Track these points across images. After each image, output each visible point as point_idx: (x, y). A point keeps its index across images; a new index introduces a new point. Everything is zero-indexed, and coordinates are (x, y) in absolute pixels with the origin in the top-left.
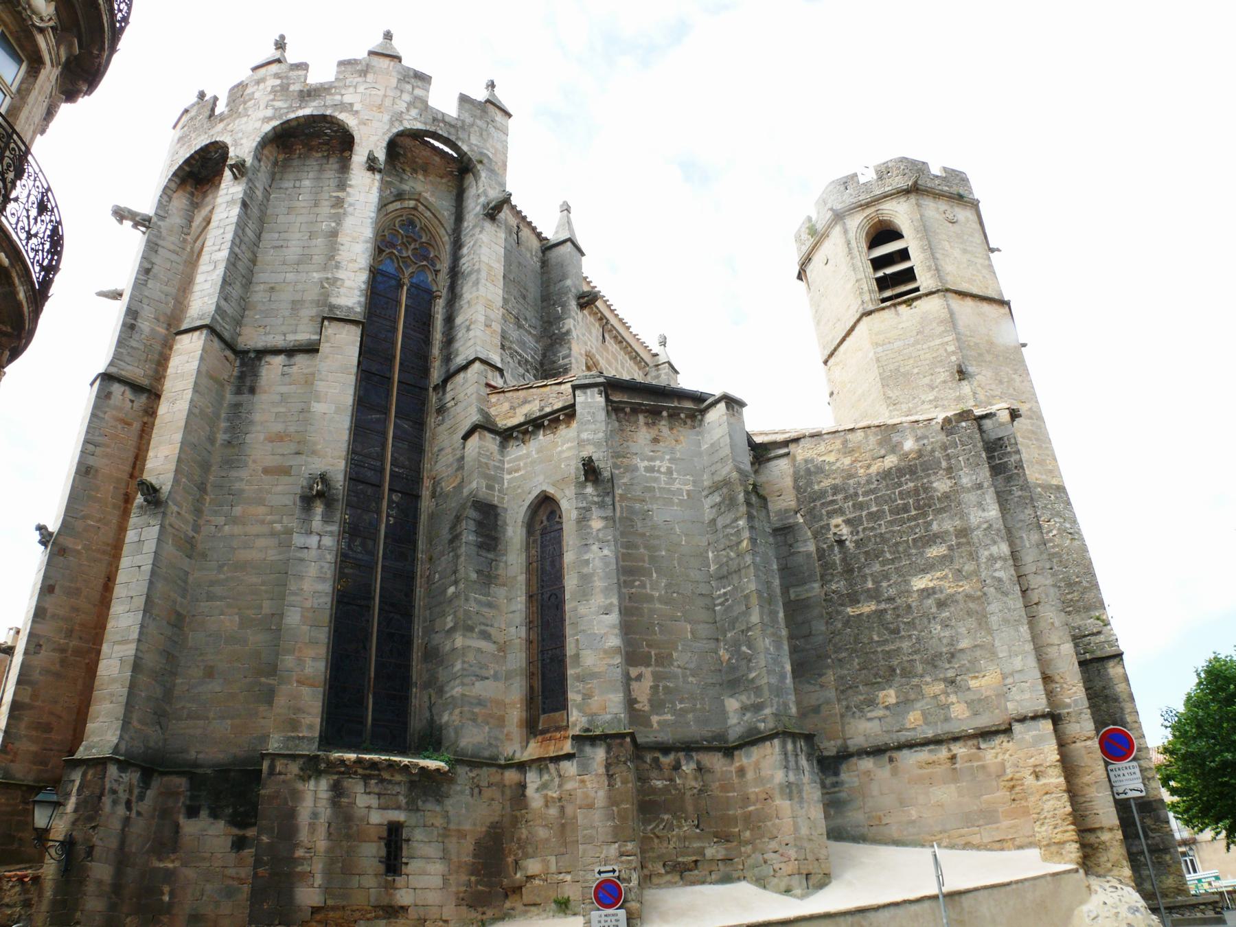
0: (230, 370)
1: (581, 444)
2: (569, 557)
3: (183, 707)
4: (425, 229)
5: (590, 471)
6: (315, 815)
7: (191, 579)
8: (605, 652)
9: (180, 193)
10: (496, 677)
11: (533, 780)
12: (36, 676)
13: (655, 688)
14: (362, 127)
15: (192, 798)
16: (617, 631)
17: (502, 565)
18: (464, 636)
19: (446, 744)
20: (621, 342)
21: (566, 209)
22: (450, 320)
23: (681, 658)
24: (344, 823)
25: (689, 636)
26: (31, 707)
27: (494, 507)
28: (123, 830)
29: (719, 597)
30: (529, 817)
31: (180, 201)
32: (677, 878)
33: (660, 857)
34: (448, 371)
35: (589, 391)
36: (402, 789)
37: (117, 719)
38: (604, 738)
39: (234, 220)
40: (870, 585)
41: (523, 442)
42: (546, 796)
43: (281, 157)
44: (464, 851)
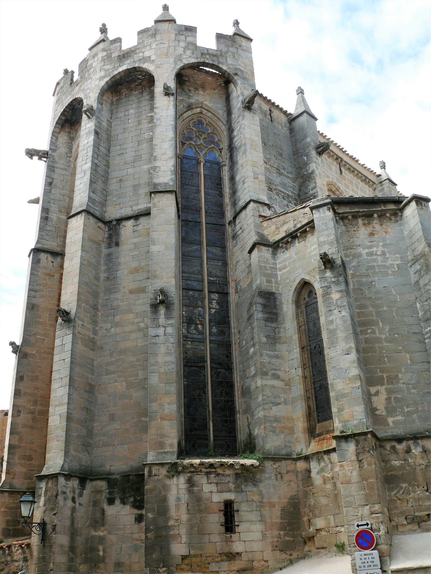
0: (102, 233)
1: (320, 245)
2: (322, 320)
3: (100, 440)
4: (209, 124)
5: (327, 262)
6: (178, 499)
7: (95, 363)
8: (350, 379)
9: (62, 134)
10: (285, 402)
11: (314, 466)
12: (20, 429)
13: (388, 399)
14: (157, 70)
15: (110, 493)
16: (356, 365)
17: (282, 330)
18: (262, 379)
19: (258, 448)
21: (300, 92)
22: (232, 179)
23: (404, 377)
24: (197, 504)
25: (409, 362)
26: (19, 447)
27: (272, 294)
28: (72, 515)
29: (427, 333)
30: (314, 491)
31: (63, 138)
32: (416, 527)
33: (402, 513)
34: (235, 211)
35: (321, 210)
36: (231, 479)
37: (61, 450)
38: (354, 436)
39: (92, 143)
41: (287, 249)
42: (323, 476)
43: (115, 99)
44: (275, 516)
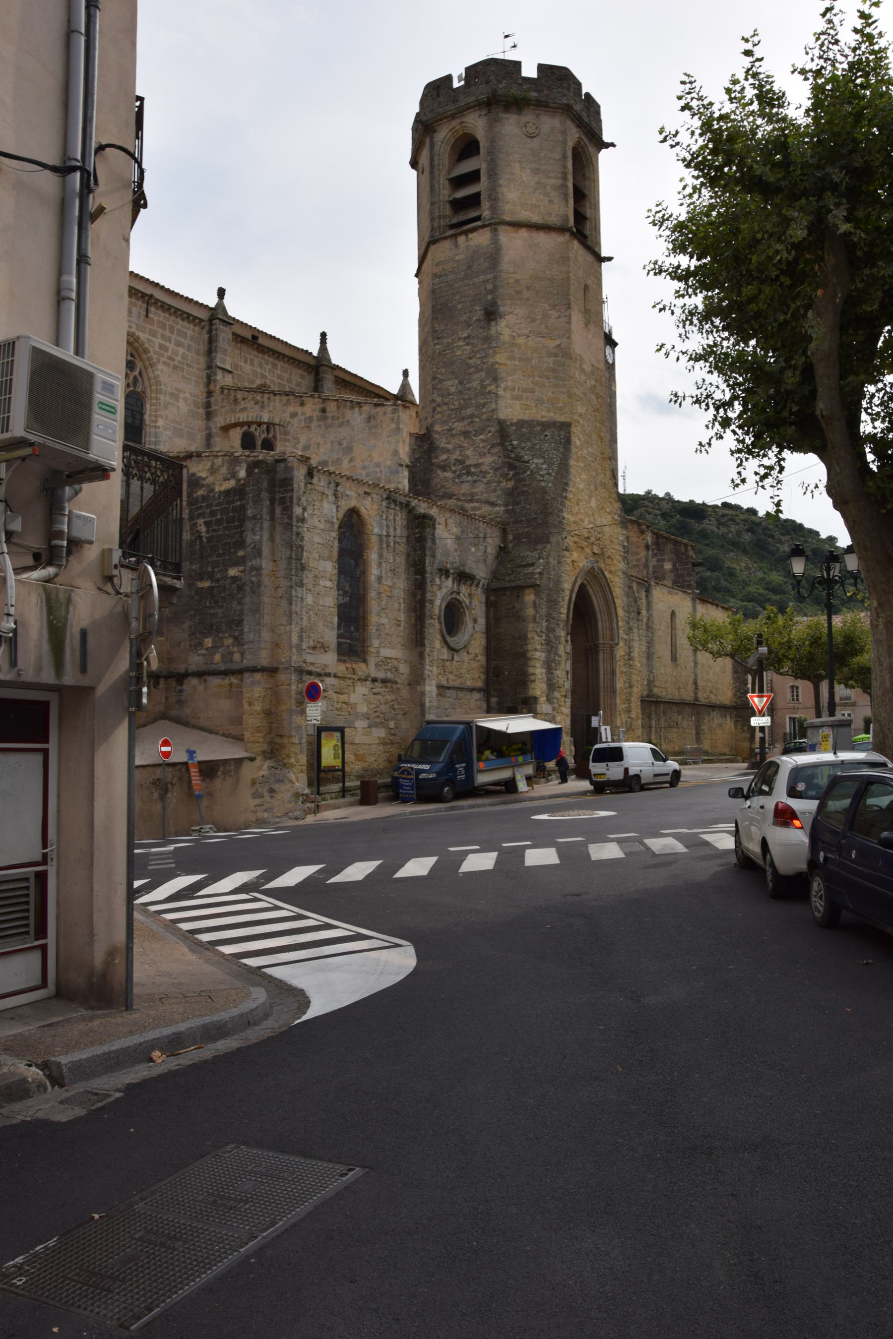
20: (168, 309)
40: (210, 569)
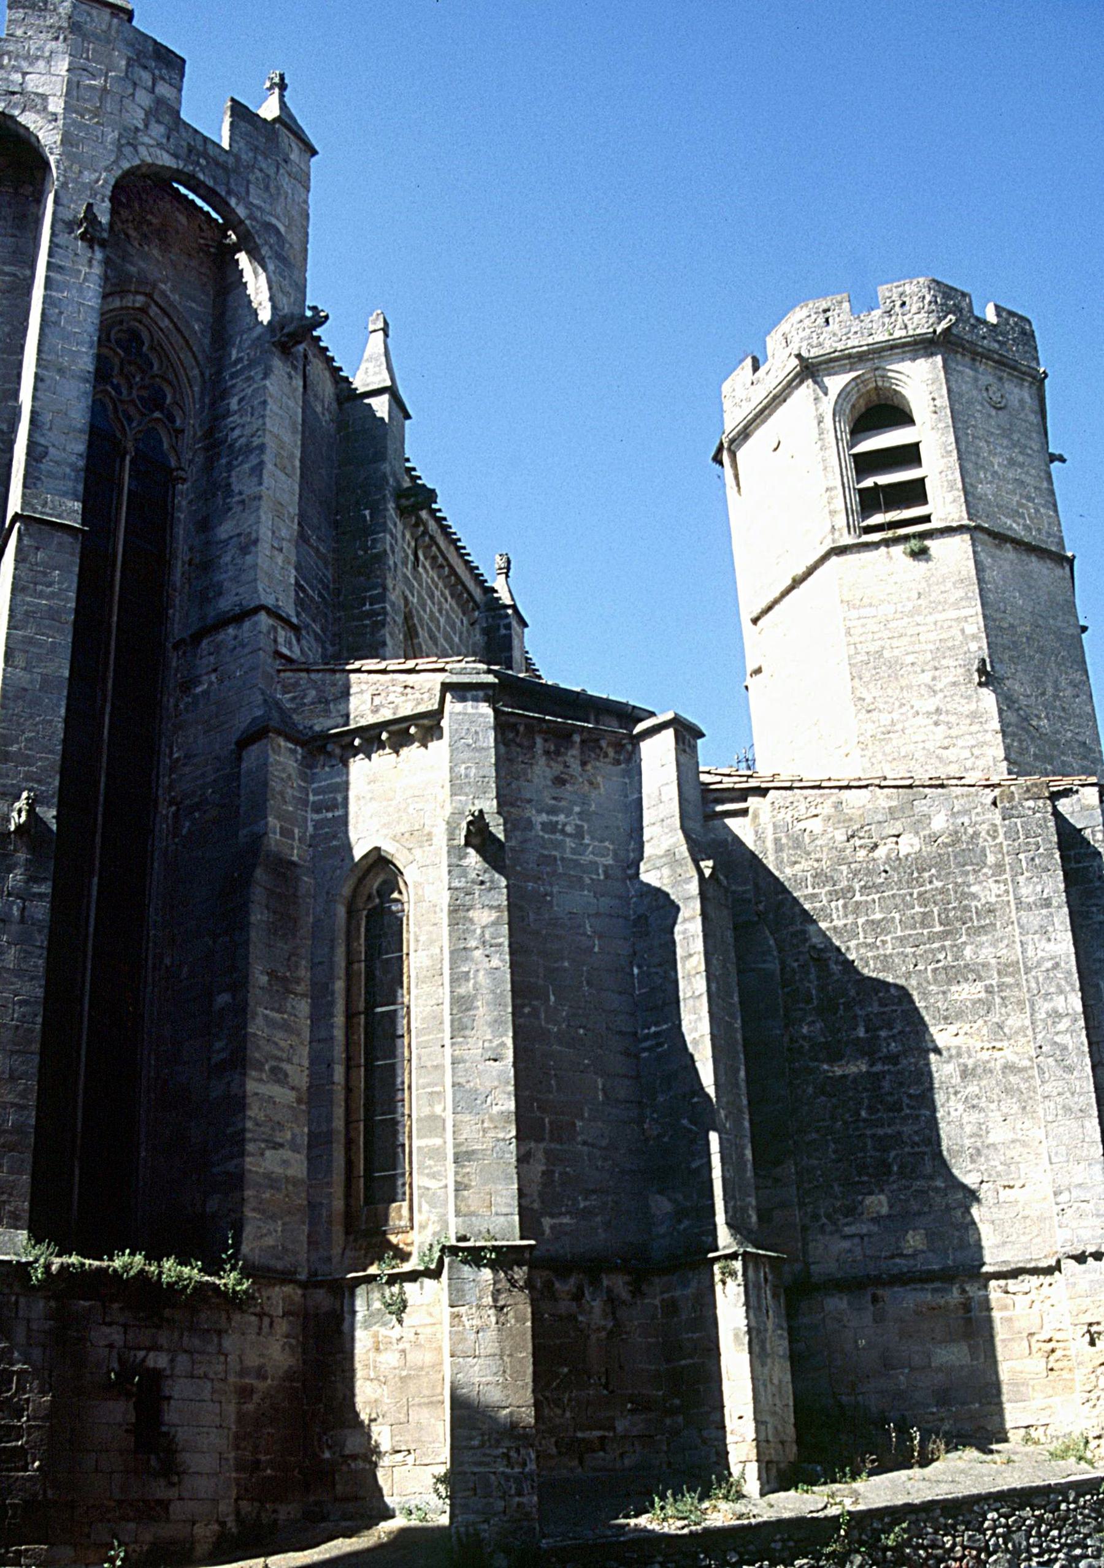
29: (647, 1037)
40: (861, 1033)
